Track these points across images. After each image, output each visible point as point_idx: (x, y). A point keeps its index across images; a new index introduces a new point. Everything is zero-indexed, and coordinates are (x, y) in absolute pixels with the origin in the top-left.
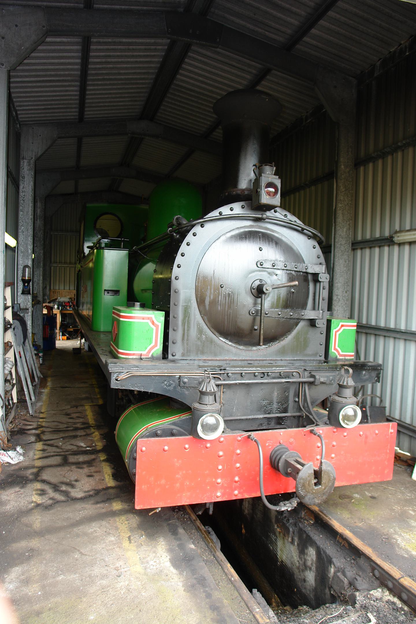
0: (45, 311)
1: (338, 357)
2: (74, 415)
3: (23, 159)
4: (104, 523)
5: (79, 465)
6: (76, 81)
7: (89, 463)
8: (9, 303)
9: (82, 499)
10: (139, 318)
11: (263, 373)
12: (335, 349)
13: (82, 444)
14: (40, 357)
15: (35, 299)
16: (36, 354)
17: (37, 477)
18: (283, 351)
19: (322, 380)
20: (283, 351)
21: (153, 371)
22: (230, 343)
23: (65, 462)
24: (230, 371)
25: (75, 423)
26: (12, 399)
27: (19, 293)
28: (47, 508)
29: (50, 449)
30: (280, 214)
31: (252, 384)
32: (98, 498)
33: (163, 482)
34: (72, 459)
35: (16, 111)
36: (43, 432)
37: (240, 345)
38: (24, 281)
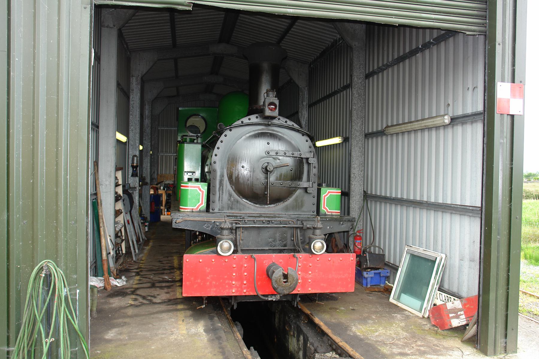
0: (152, 192)
1: (327, 213)
2: (165, 262)
3: (133, 76)
4: (170, 314)
5: (161, 288)
6: (168, 23)
7: (168, 287)
8: (120, 182)
9: (159, 303)
10: (191, 187)
11: (269, 221)
12: (324, 208)
13: (166, 277)
14: (146, 226)
15: (142, 180)
16: (142, 223)
17: (133, 293)
18: (287, 209)
19: (308, 226)
20: (287, 209)
21: (197, 218)
22: (250, 203)
23: (153, 286)
24: (247, 219)
25: (164, 266)
26: (122, 250)
27: (130, 176)
28: (137, 306)
29: (144, 279)
30: (282, 120)
31: (260, 227)
32: (169, 303)
33: (199, 281)
34: (157, 285)
35: (127, 44)
36: (141, 271)
37: (256, 204)
38: (133, 167)
